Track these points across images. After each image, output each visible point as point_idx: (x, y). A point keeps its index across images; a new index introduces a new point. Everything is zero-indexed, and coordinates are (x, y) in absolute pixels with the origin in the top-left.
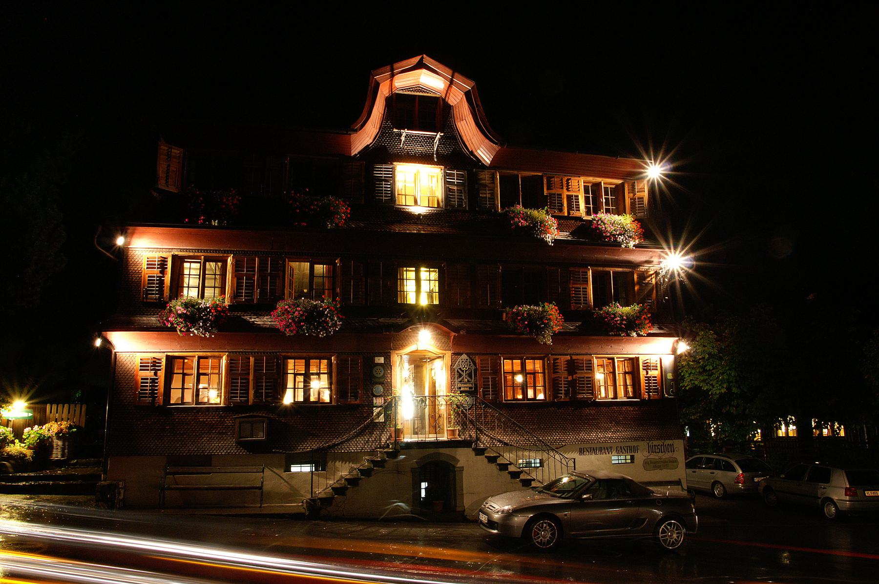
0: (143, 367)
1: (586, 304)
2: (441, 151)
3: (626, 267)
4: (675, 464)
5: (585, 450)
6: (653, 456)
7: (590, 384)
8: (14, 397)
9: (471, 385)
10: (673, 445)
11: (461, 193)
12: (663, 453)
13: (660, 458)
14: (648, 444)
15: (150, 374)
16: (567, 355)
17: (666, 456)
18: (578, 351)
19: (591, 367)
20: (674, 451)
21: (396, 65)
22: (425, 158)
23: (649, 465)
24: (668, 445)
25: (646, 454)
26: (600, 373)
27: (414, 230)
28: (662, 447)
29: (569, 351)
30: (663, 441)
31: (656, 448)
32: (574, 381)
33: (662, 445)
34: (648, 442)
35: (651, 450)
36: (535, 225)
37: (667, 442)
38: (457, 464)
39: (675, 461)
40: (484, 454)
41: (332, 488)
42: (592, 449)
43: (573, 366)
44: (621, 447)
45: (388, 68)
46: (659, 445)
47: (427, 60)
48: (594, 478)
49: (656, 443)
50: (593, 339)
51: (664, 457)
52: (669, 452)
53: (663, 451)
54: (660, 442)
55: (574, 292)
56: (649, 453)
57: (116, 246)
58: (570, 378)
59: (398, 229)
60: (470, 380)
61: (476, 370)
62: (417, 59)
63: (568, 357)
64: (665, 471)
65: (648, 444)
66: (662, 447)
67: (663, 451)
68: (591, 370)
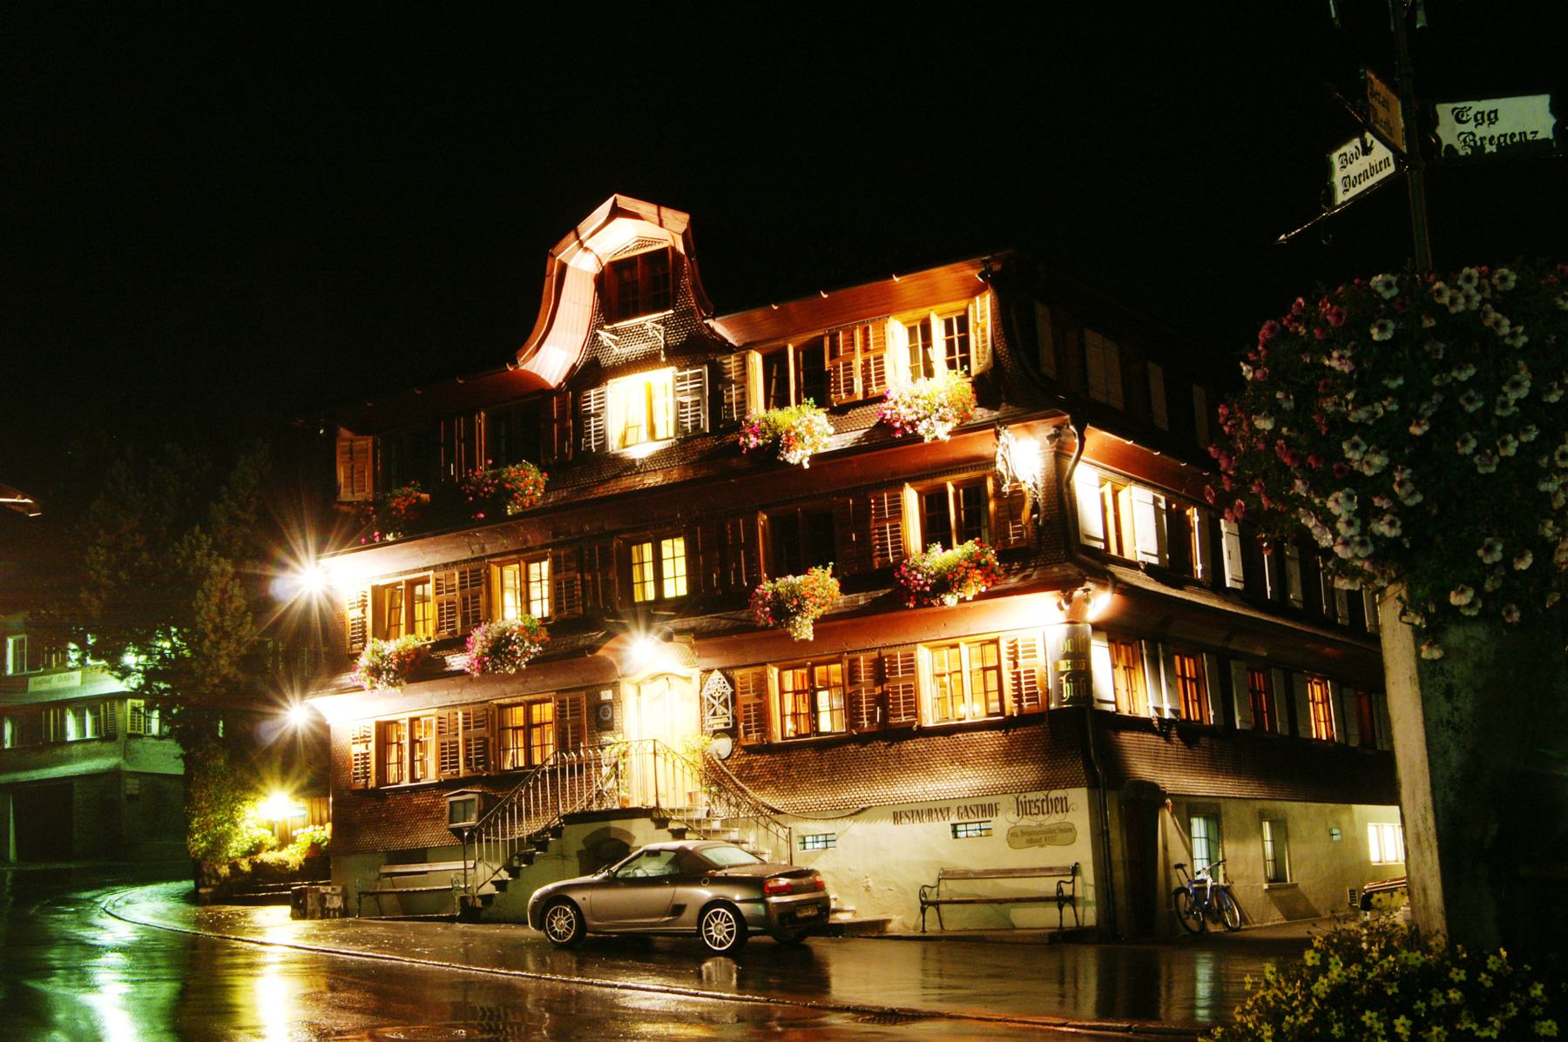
0: (355, 741)
1: (900, 553)
2: (672, 341)
3: (974, 468)
4: (1069, 834)
5: (903, 815)
6: (1027, 821)
7: (911, 697)
8: (269, 782)
9: (726, 720)
10: (1066, 798)
11: (698, 405)
12: (1046, 816)
13: (1041, 825)
14: (1017, 799)
15: (360, 749)
16: (872, 649)
17: (1053, 819)
18: (888, 642)
19: (913, 666)
20: (1067, 811)
21: (582, 227)
22: (648, 361)
23: (1019, 838)
24: (1057, 798)
25: (1013, 817)
26: (1078, 656)
27: (653, 480)
28: (1045, 804)
29: (875, 644)
30: (1046, 792)
31: (1033, 805)
32: (884, 695)
33: (1043, 800)
34: (1017, 795)
35: (1023, 809)
36: (777, 438)
37: (1054, 794)
38: (632, 841)
39: (1070, 829)
40: (667, 826)
41: (492, 882)
42: (915, 814)
43: (880, 671)
44: (966, 807)
45: (572, 235)
46: (1037, 800)
47: (625, 202)
48: (364, 852)
49: (1032, 796)
50: (927, 614)
51: (1047, 823)
52: (1057, 812)
53: (1045, 811)
54: (1041, 795)
55: (877, 531)
56: (1018, 815)
57: (280, 610)
58: (878, 690)
59: (616, 487)
60: (726, 711)
61: (733, 695)
62: (607, 205)
63: (875, 654)
64: (1049, 848)
65: (1017, 799)
66: (1045, 804)
67: (1045, 811)
68: (913, 672)
